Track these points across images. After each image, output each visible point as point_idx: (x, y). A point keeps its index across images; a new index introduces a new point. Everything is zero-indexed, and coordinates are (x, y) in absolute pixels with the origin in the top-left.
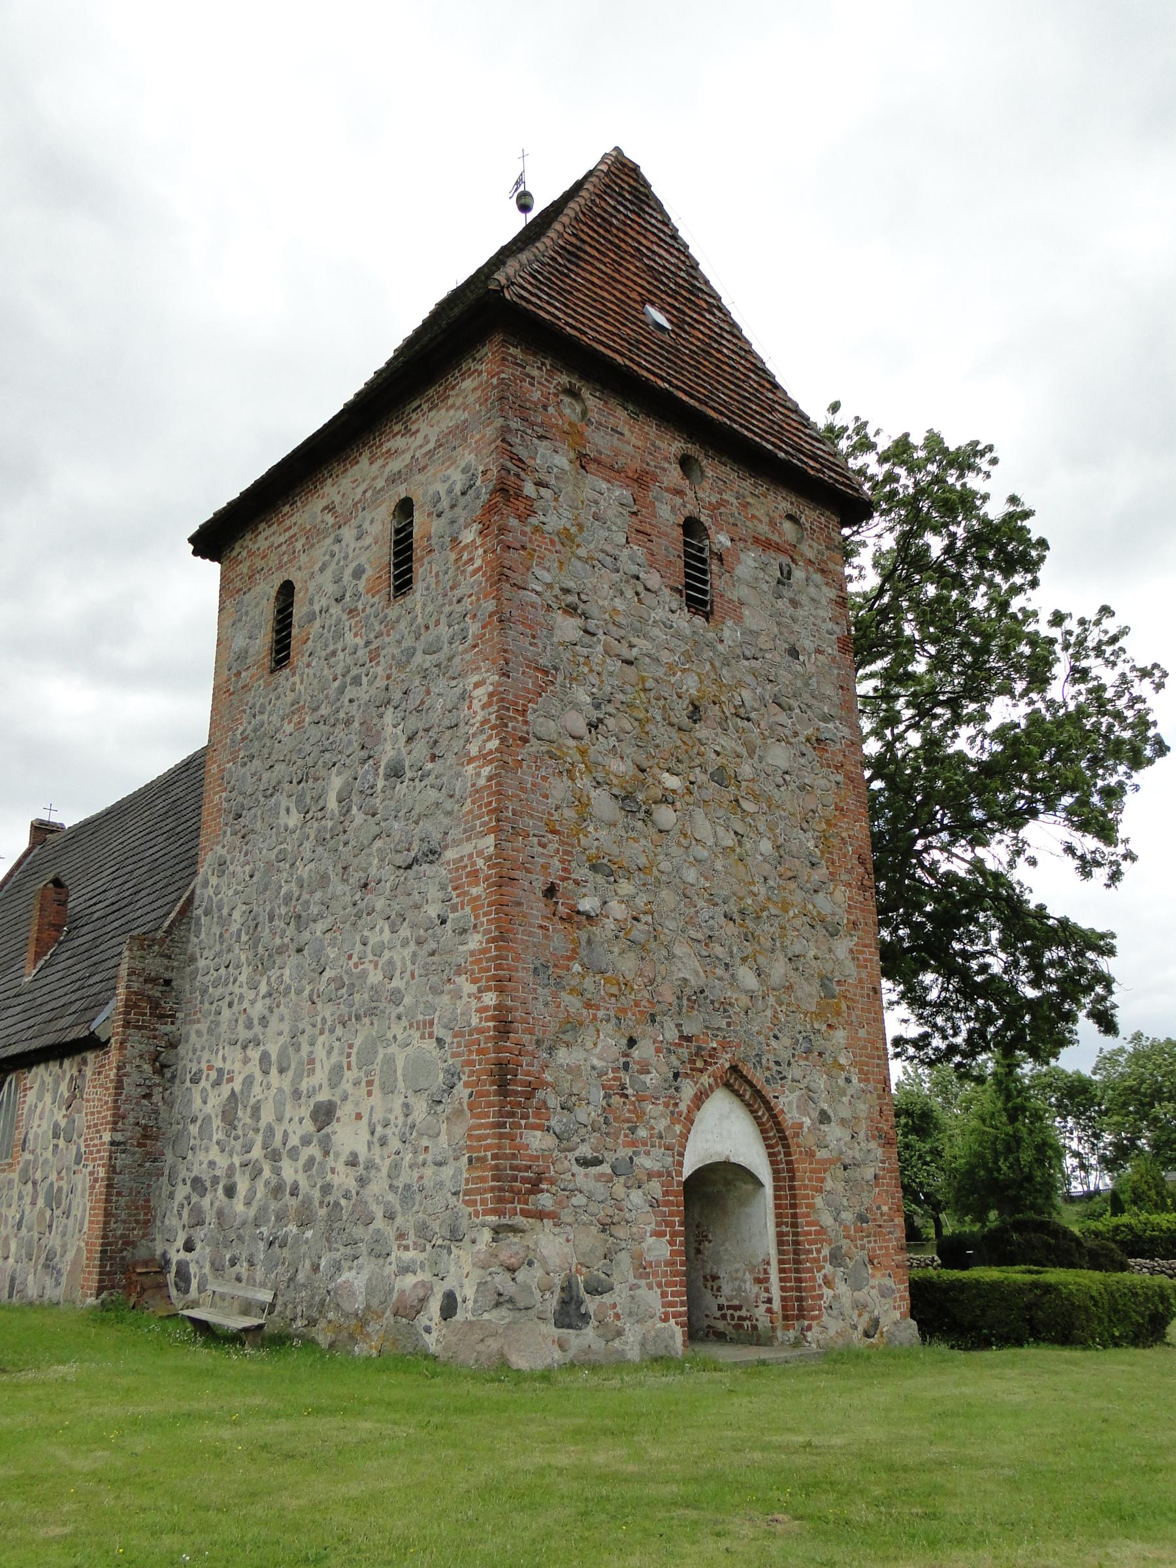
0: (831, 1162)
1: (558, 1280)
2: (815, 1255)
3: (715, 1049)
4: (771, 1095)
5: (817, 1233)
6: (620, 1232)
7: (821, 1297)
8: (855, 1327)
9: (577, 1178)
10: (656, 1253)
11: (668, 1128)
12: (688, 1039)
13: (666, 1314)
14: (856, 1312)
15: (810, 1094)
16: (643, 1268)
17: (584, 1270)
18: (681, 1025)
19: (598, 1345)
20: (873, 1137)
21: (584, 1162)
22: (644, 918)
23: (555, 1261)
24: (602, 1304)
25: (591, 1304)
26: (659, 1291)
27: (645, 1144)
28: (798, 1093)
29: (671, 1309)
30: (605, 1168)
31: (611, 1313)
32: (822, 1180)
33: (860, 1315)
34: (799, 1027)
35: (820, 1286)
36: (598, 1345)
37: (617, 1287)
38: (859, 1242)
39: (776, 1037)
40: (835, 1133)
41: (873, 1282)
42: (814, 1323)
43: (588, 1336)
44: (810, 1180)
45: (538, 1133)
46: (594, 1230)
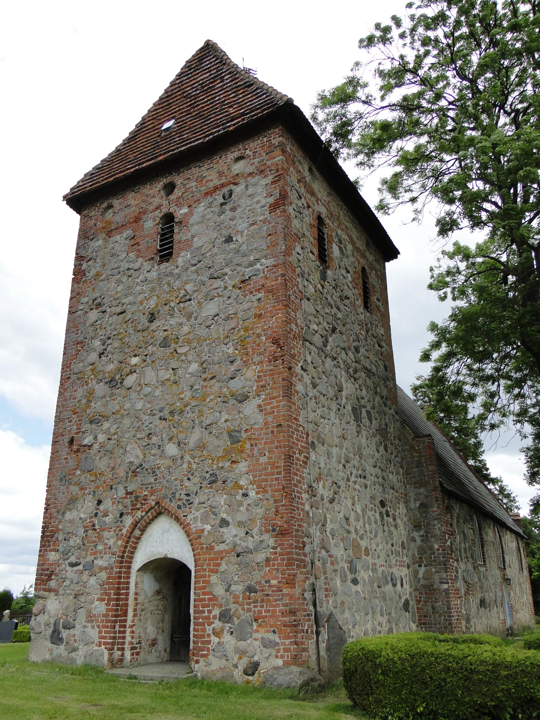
0: (227, 552)
1: (52, 621)
2: (206, 614)
3: (146, 495)
4: (182, 515)
5: (210, 600)
6: (82, 598)
7: (209, 642)
8: (236, 666)
9: (68, 573)
10: (98, 610)
11: (115, 543)
12: (131, 493)
13: (100, 642)
14: (238, 655)
15: (213, 510)
16: (91, 618)
17: (64, 617)
18: (127, 487)
19: (65, 654)
20: (267, 531)
21: (72, 565)
22: (113, 437)
23: (53, 612)
24: (69, 634)
25: (64, 634)
26: (98, 630)
27: (100, 553)
28: (202, 510)
29: (103, 640)
30: (80, 567)
31: (72, 639)
32: (219, 565)
33: (240, 658)
34: (207, 469)
35: (209, 635)
36: (65, 654)
37: (77, 626)
38: (246, 607)
39: (189, 479)
40: (231, 533)
41: (255, 635)
42: (201, 660)
43: (61, 649)
44: (209, 565)
45: (53, 553)
46: (71, 597)
